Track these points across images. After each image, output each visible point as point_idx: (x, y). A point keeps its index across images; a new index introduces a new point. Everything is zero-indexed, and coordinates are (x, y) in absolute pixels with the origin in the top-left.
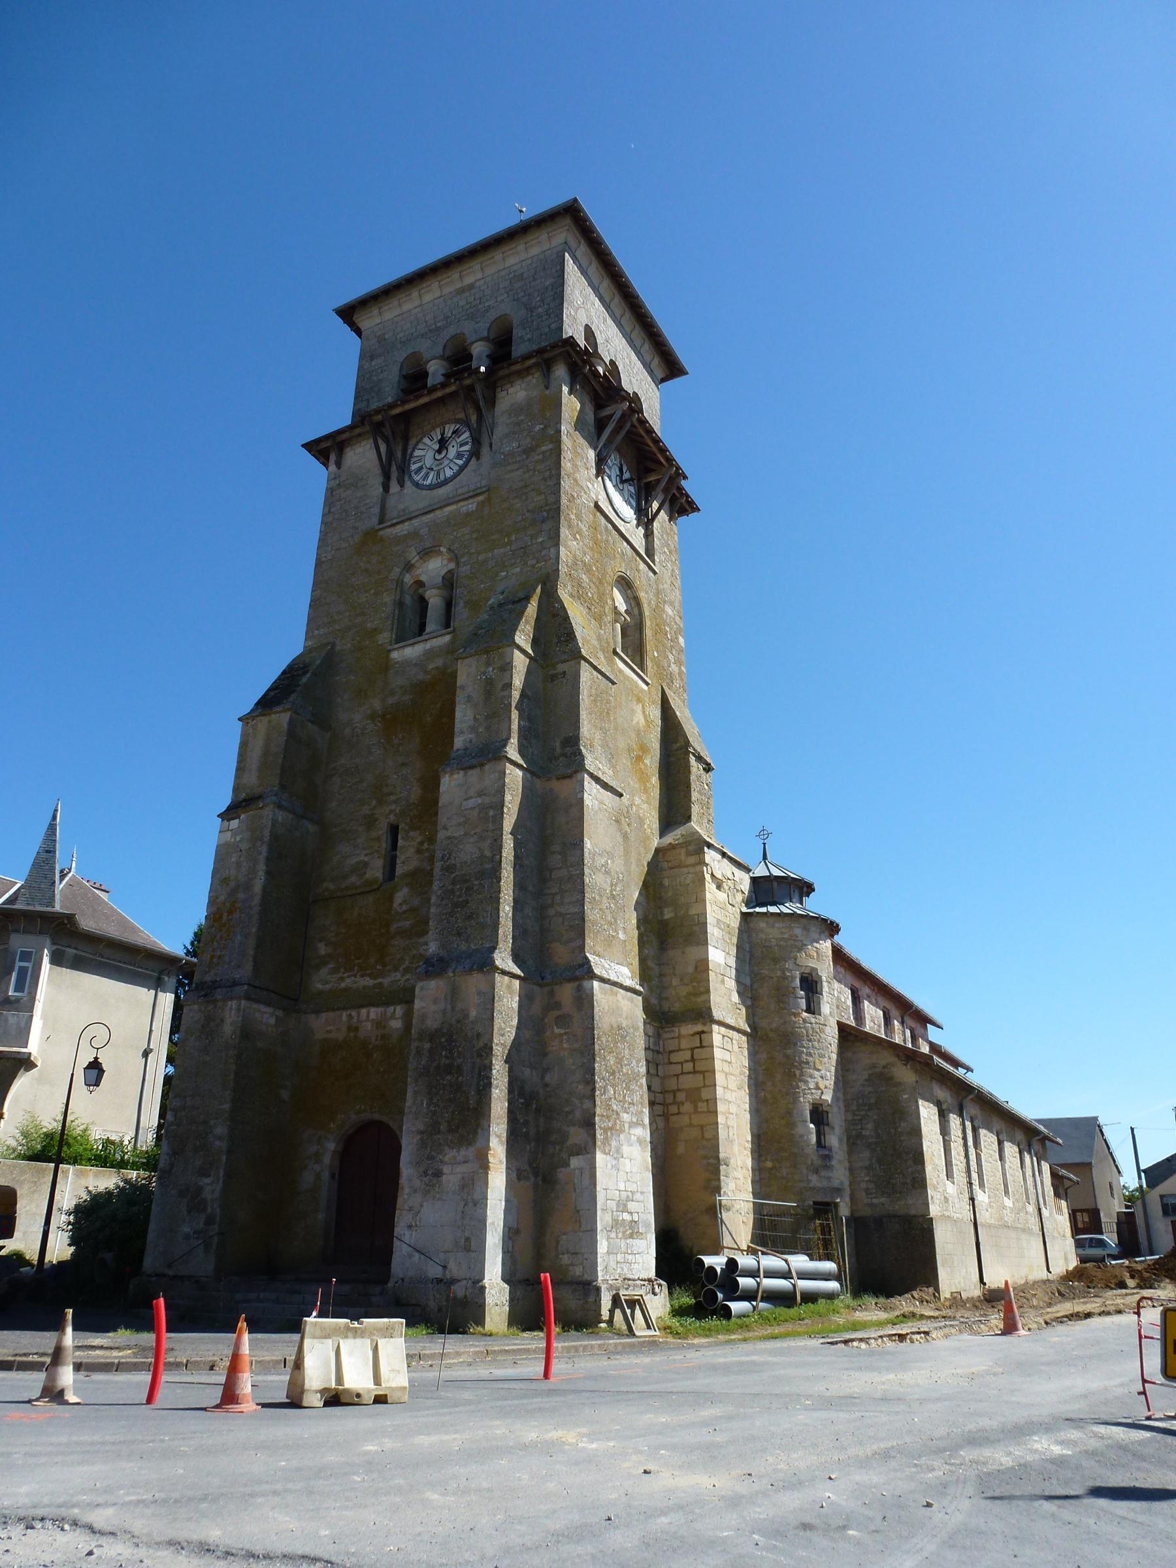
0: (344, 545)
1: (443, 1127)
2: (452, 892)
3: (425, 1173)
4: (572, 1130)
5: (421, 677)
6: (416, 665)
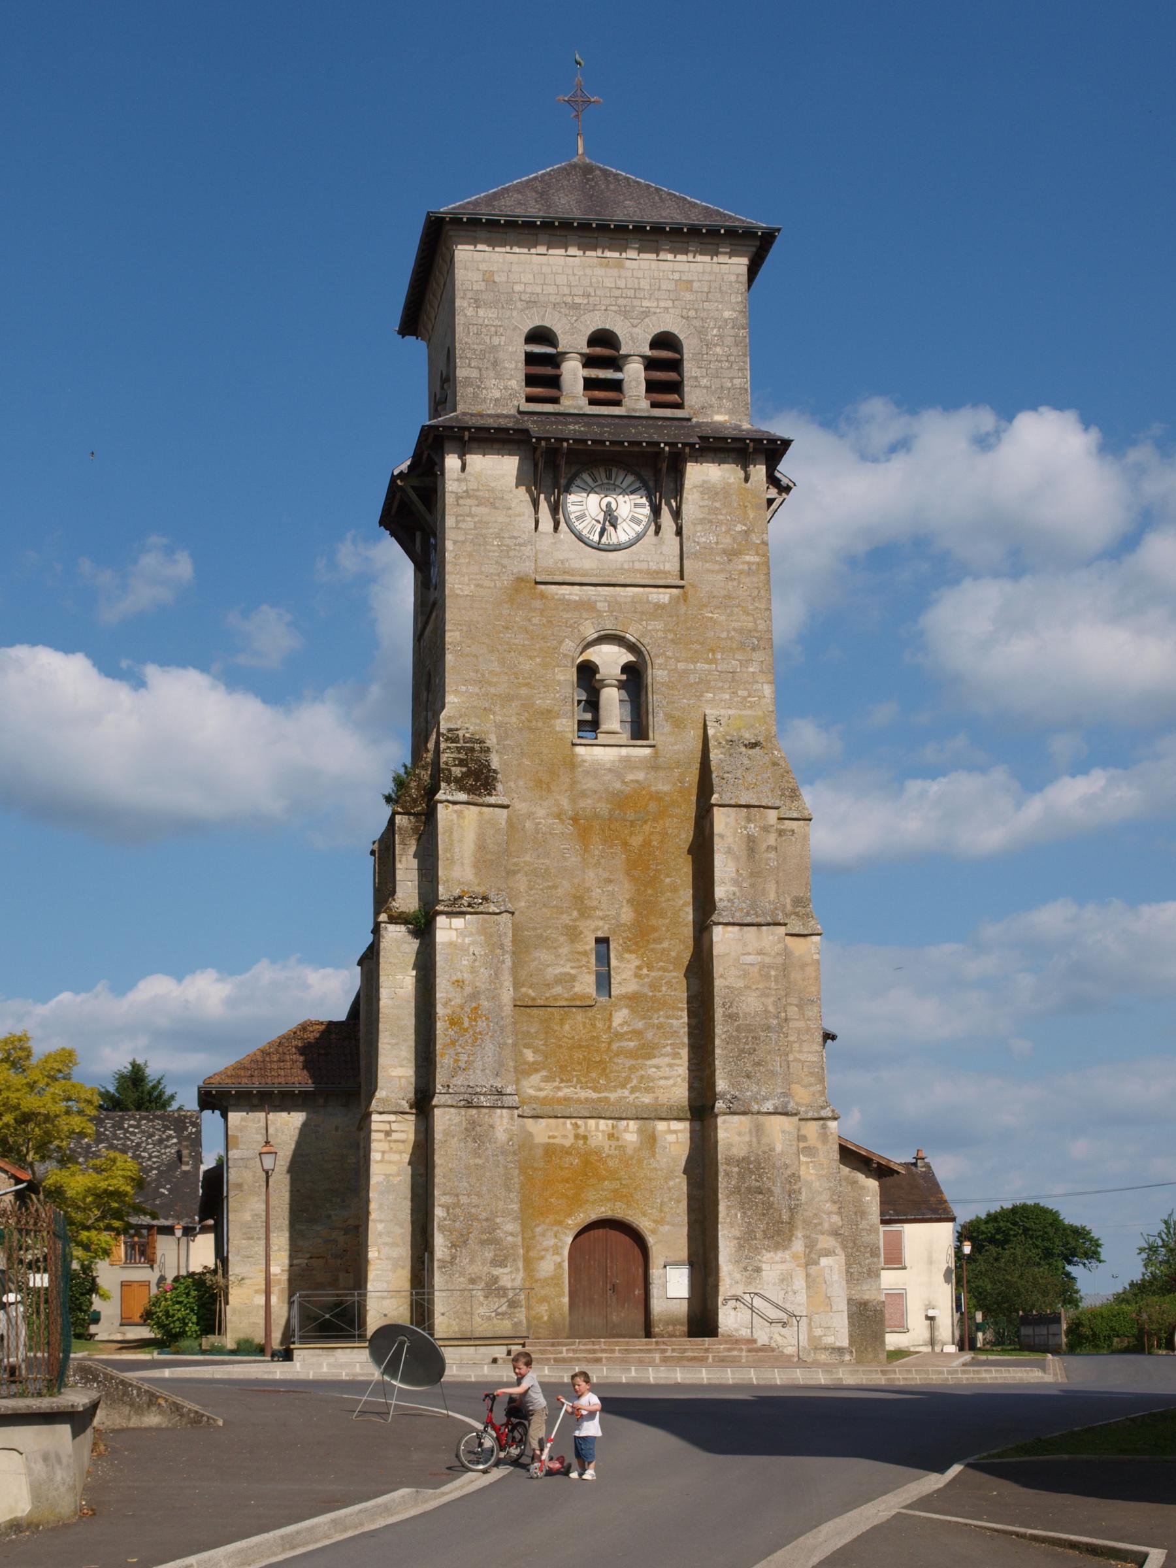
0: (487, 583)
1: (759, 1235)
3: (746, 1269)
4: (821, 1237)
5: (618, 785)
6: (610, 770)
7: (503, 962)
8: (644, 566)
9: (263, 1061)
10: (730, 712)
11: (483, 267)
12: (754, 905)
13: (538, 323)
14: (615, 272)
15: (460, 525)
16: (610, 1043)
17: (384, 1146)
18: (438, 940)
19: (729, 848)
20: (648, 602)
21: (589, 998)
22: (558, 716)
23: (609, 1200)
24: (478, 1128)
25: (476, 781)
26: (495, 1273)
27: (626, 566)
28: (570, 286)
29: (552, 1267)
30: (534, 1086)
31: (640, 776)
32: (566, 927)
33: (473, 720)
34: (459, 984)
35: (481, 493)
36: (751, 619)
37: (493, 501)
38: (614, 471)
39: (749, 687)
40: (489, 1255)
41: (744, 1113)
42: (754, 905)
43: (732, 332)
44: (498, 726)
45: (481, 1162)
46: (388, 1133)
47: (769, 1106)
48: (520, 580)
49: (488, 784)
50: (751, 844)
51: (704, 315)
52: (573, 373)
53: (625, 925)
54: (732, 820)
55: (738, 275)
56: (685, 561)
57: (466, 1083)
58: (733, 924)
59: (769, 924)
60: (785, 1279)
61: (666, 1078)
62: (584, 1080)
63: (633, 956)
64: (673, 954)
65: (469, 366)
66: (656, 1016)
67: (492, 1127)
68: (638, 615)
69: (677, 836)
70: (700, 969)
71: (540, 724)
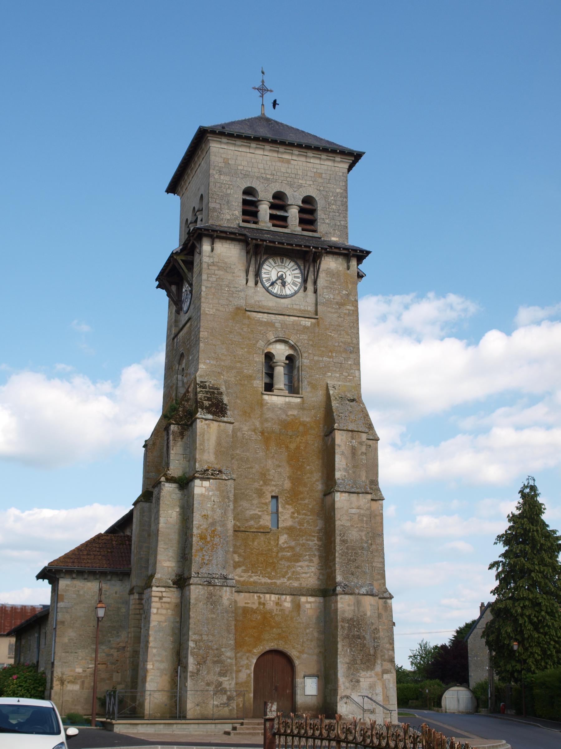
1: (359, 662)
2: (347, 553)
3: (352, 681)
5: (284, 417)
6: (280, 408)
7: (229, 506)
8: (298, 307)
9: (79, 554)
10: (339, 383)
11: (224, 156)
12: (355, 483)
13: (249, 185)
14: (286, 165)
15: (209, 279)
16: (277, 553)
17: (158, 605)
18: (195, 492)
19: (343, 452)
20: (300, 325)
21: (267, 528)
22: (255, 379)
23: (275, 639)
24: (214, 597)
25: (217, 409)
26: (220, 680)
27: (289, 307)
28: (265, 169)
29: (245, 676)
30: (238, 575)
31: (295, 412)
32: (256, 489)
33: (213, 378)
34: (205, 517)
35: (220, 264)
36: (349, 337)
37: (226, 268)
38: (285, 259)
39: (348, 371)
40: (218, 670)
41: (351, 594)
42: (355, 483)
43: (340, 199)
44: (225, 382)
45: (214, 616)
46: (161, 598)
47: (363, 590)
48: (238, 309)
49: (223, 411)
50: (354, 451)
51: (327, 189)
52: (264, 210)
53: (286, 490)
54: (344, 437)
55: (343, 173)
56: (318, 306)
57: (208, 572)
58: (346, 492)
59: (363, 493)
60: (372, 687)
61: (306, 573)
62: (264, 572)
63: (290, 507)
64: (310, 506)
65: (215, 202)
66: (301, 539)
67: (221, 597)
68: (295, 331)
69: (313, 445)
70: (327, 514)
71: (246, 382)
